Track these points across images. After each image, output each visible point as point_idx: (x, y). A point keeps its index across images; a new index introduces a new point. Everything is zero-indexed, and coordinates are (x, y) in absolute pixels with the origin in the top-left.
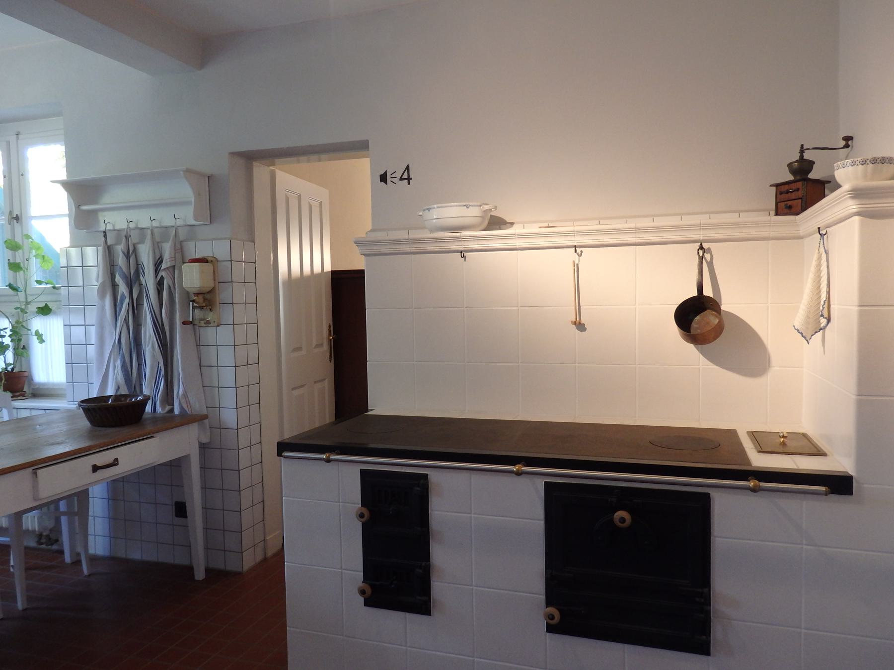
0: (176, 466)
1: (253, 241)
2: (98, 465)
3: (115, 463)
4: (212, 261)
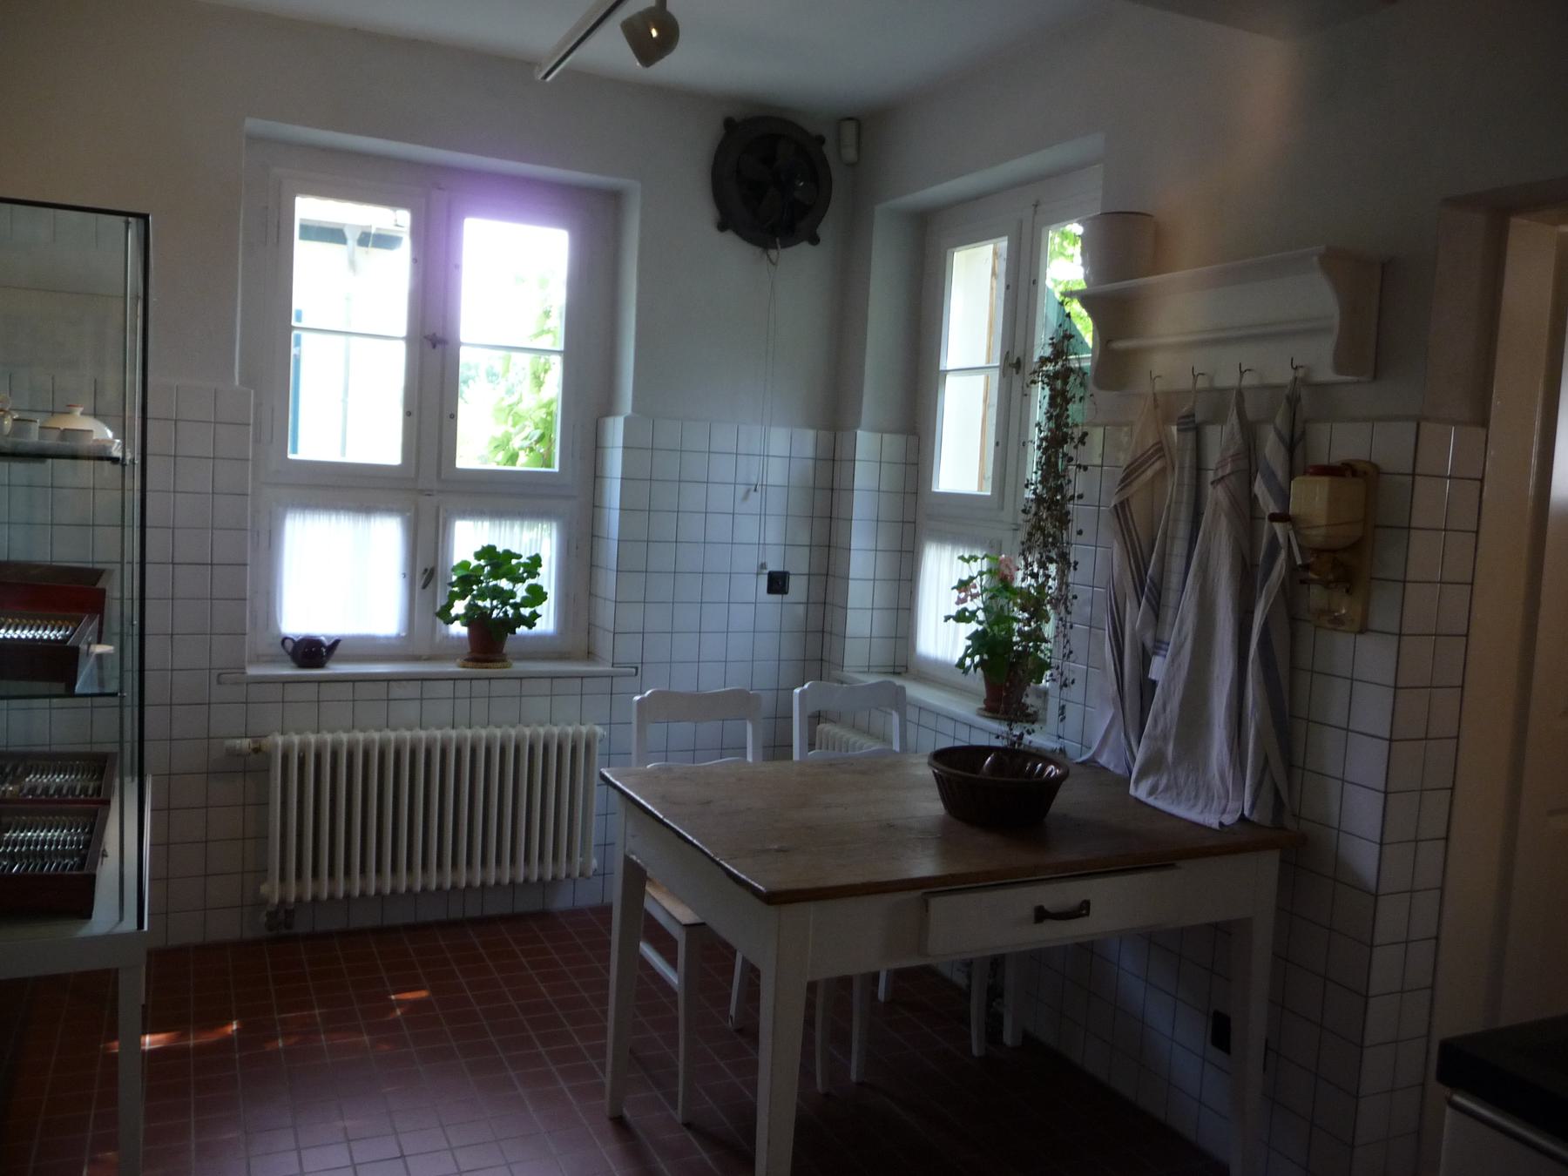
0: (1224, 934)
1: (1484, 423)
2: (1046, 907)
3: (1083, 909)
4: (1365, 473)
